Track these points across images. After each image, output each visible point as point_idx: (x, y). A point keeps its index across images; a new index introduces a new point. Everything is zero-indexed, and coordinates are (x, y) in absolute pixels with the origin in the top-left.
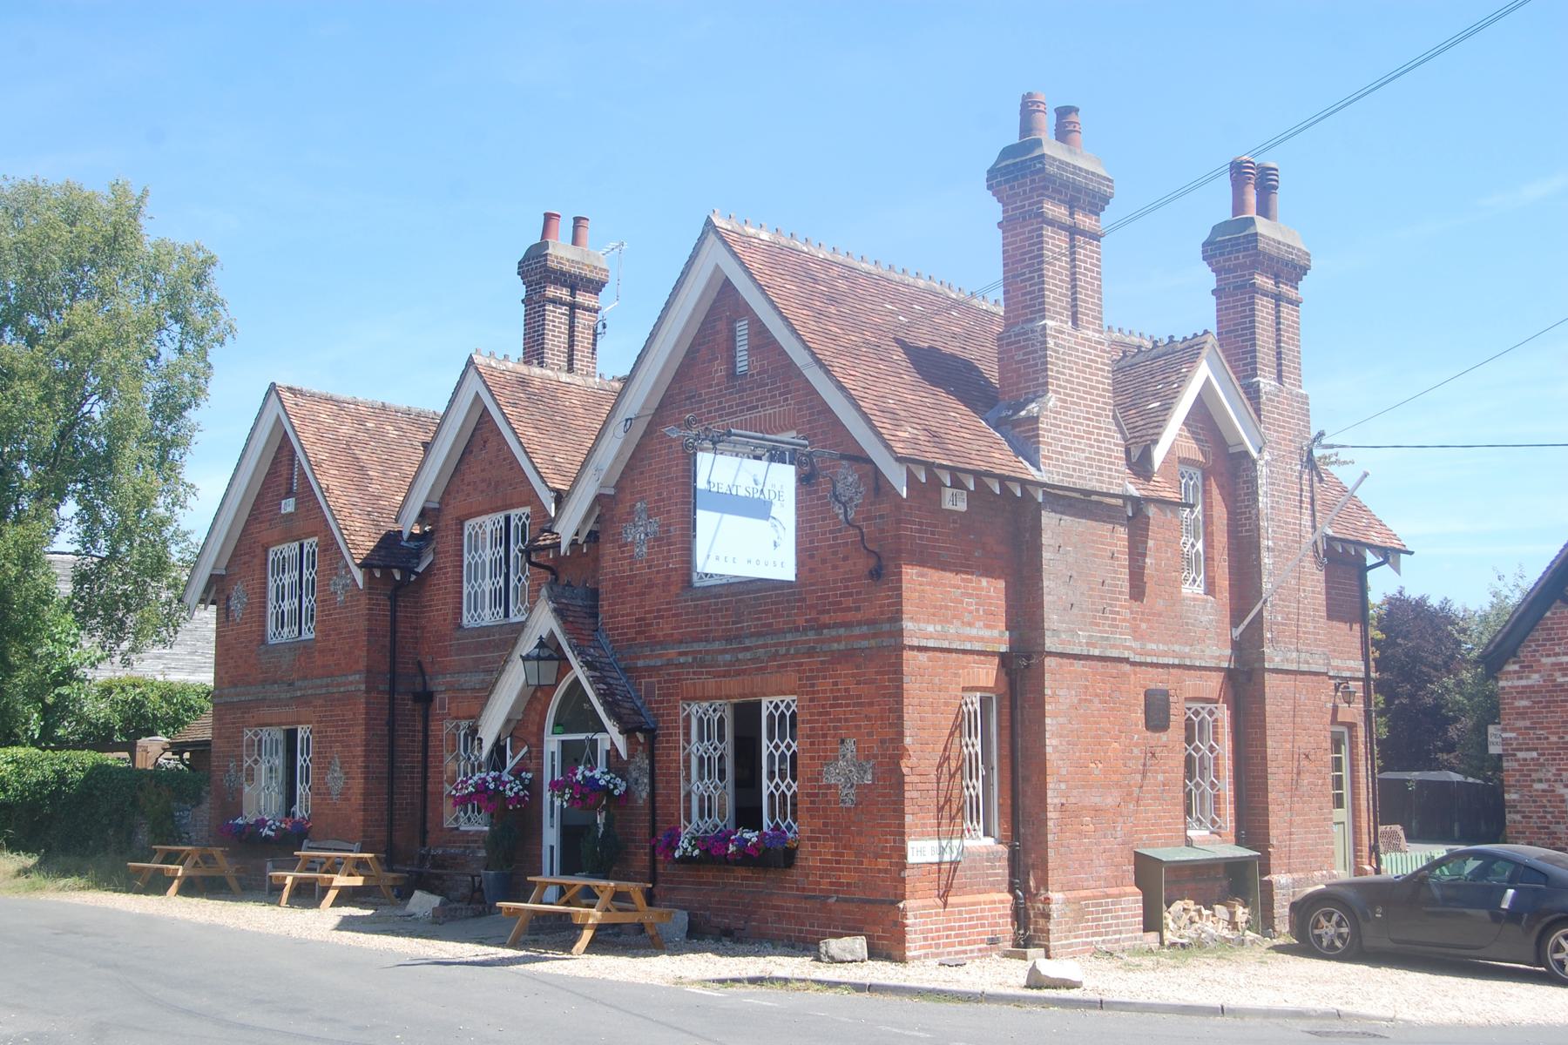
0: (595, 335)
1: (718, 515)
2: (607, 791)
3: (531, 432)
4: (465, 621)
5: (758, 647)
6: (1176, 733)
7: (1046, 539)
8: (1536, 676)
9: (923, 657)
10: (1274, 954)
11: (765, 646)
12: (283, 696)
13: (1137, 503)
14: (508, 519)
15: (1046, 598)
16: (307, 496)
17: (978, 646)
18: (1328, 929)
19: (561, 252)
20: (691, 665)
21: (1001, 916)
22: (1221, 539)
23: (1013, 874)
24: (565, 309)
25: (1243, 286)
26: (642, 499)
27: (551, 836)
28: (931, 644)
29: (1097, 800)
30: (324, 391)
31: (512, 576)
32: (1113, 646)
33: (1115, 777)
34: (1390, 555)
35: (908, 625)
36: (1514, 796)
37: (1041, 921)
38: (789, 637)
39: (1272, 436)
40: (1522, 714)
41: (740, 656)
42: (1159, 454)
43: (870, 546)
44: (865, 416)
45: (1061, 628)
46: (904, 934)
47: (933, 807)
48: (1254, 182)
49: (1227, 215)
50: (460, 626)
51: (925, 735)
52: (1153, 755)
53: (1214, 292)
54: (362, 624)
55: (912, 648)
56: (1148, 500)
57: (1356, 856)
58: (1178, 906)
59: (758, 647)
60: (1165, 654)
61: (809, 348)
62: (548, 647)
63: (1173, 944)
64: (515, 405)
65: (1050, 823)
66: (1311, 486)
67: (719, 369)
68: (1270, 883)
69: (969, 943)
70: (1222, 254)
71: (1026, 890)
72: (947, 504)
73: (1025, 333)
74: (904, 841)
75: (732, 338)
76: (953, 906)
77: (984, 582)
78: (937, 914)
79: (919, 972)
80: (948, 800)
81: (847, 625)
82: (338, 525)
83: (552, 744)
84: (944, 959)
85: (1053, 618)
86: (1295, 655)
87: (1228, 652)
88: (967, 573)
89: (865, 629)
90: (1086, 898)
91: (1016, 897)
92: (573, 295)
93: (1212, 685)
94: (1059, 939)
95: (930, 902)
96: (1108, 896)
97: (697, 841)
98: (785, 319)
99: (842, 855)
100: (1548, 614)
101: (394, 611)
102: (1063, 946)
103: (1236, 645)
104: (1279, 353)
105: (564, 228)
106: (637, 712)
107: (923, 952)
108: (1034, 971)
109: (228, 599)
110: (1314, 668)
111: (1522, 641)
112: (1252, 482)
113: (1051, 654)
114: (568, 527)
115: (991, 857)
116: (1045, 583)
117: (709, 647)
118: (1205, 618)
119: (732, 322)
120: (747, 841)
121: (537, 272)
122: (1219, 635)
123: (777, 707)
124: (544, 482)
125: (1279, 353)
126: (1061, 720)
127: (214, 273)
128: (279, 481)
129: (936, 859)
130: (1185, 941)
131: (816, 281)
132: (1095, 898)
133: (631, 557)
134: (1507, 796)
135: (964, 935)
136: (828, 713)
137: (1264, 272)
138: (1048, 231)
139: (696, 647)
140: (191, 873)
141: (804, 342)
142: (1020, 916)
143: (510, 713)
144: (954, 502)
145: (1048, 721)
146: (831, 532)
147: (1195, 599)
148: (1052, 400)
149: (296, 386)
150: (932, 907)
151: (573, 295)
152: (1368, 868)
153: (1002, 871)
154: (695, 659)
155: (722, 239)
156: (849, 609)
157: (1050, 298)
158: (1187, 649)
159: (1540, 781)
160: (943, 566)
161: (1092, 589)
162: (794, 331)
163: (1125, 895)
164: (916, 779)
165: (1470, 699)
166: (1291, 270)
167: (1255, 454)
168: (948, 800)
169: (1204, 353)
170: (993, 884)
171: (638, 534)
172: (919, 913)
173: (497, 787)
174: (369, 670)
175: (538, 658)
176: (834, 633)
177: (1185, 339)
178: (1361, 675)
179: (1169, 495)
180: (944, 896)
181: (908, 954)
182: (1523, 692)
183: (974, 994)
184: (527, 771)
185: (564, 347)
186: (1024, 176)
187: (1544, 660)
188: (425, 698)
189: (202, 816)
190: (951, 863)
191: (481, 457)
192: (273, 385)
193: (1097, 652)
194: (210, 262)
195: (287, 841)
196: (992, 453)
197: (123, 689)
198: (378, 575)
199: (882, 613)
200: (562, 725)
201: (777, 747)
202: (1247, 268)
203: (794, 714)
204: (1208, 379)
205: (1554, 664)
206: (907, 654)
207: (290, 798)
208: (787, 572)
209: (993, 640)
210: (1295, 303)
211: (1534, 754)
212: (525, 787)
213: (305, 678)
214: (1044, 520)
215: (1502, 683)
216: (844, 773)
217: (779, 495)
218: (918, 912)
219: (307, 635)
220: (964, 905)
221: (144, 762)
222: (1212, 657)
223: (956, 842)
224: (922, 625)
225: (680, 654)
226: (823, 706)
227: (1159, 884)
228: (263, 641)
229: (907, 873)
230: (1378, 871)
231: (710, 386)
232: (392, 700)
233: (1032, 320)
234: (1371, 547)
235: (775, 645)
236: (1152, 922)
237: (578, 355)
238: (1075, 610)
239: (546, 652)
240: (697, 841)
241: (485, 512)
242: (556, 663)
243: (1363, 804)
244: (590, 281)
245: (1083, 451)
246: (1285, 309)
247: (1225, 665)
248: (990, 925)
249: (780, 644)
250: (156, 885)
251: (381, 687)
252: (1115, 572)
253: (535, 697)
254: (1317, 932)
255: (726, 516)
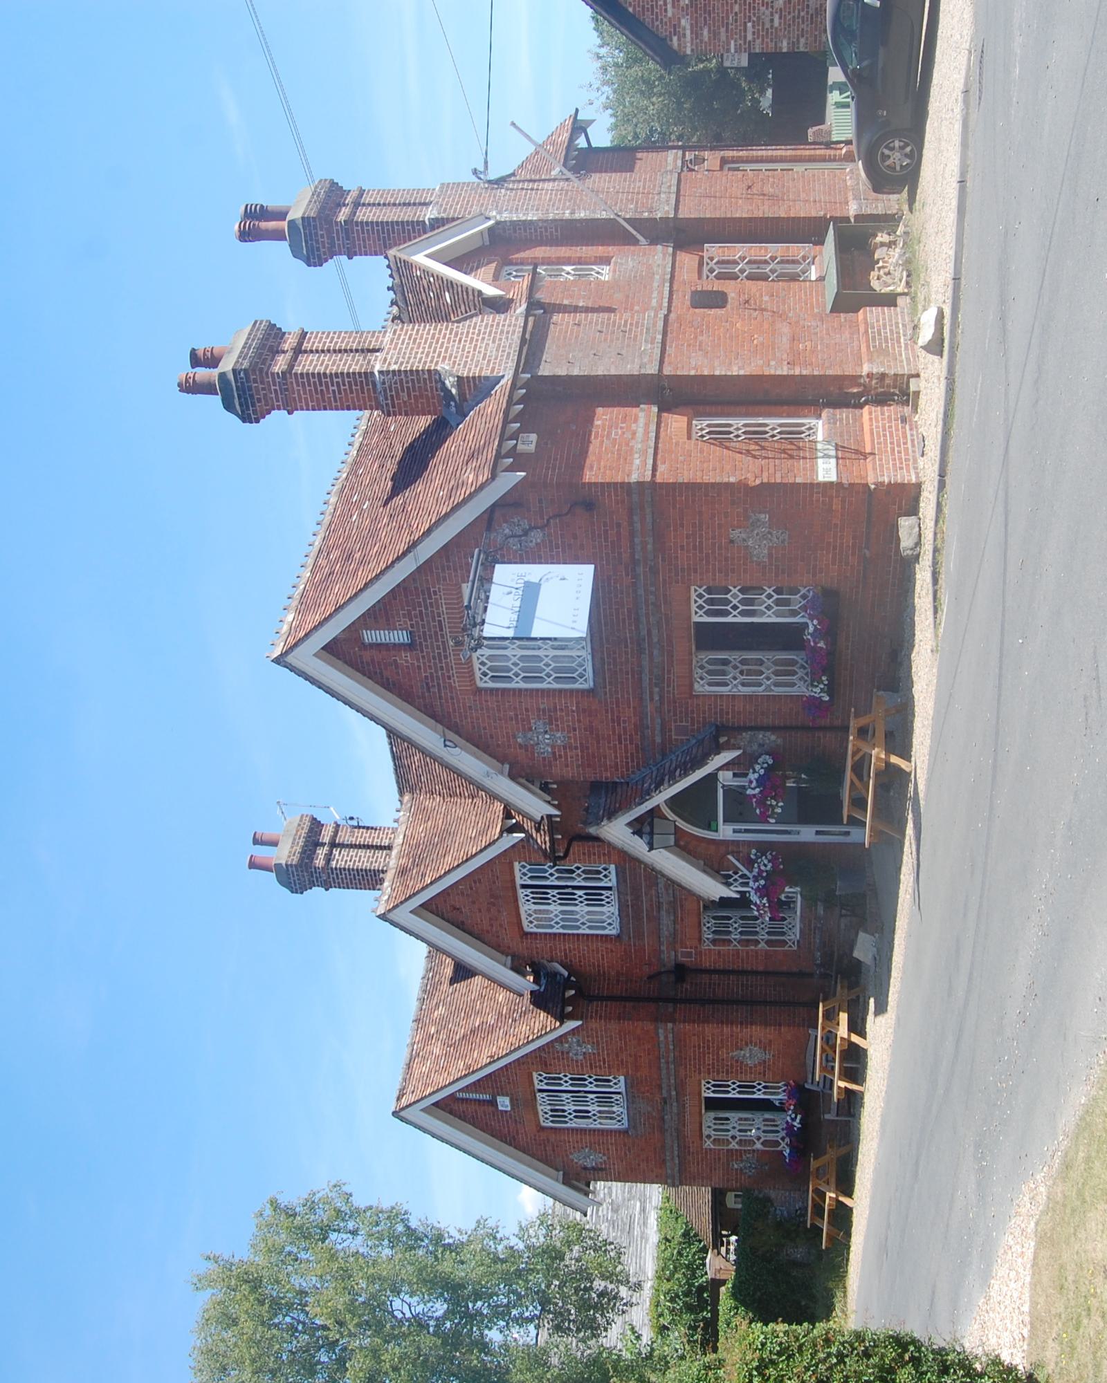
0: (359, 827)
1: (536, 621)
2: (769, 769)
3: (449, 859)
4: (614, 932)
5: (648, 622)
6: (729, 287)
7: (562, 372)
8: (683, 22)
9: (661, 468)
10: (917, 205)
11: (647, 615)
12: (675, 1110)
13: (533, 305)
14: (524, 886)
15: (613, 372)
16: (493, 1082)
17: (653, 427)
18: (896, 158)
19: (285, 854)
20: (662, 689)
21: (883, 414)
22: (564, 251)
23: (847, 406)
24: (336, 852)
25: (347, 231)
26: (514, 737)
27: (807, 834)
28: (650, 462)
29: (784, 339)
30: (401, 1071)
31: (575, 883)
32: (655, 324)
33: (766, 326)
34: (579, 127)
35: (634, 478)
36: (785, 43)
37: (887, 381)
38: (641, 592)
39: (475, 209)
40: (715, 34)
41: (655, 640)
42: (490, 291)
43: (565, 510)
44: (455, 509)
45: (640, 360)
46: (896, 484)
47: (790, 462)
48: (256, 224)
49: (284, 246)
50: (618, 937)
51: (728, 467)
52: (747, 302)
53: (350, 258)
54: (614, 1026)
55: (654, 475)
56: (530, 296)
57: (835, 160)
58: (875, 284)
59: (648, 622)
60: (661, 293)
61: (393, 562)
62: (641, 827)
63: (908, 284)
64: (423, 876)
65: (804, 373)
66: (519, 181)
67: (405, 658)
68: (856, 217)
69: (905, 437)
70: (318, 249)
71: (860, 395)
72: (532, 448)
73: (385, 390)
74: (819, 484)
75: (379, 646)
76: (873, 447)
77: (597, 423)
78: (881, 460)
79: (927, 470)
80: (784, 451)
81: (632, 534)
82: (524, 1045)
83: (726, 832)
84: (918, 455)
85: (630, 368)
86: (663, 196)
87: (659, 247)
88: (590, 435)
89: (636, 518)
90: (868, 347)
91: (866, 403)
92: (323, 845)
93: (687, 261)
94: (902, 367)
95: (870, 466)
96: (866, 332)
97: (814, 680)
98: (366, 585)
99: (829, 543)
100: (631, 10)
101: (601, 998)
102: (908, 364)
103: (654, 241)
104: (404, 204)
105: (263, 852)
106: (700, 742)
107: (912, 472)
108: (928, 348)
109: (585, 1168)
110: (674, 182)
111: (653, 33)
112: (515, 225)
113: (660, 369)
114: (536, 806)
115: (832, 421)
116: (600, 373)
117: (647, 671)
118: (631, 263)
119: (364, 647)
120: (816, 629)
121: (303, 874)
122: (645, 254)
123: (700, 607)
124: (495, 841)
125: (404, 204)
126: (716, 363)
127: (284, 1200)
128: (483, 1111)
129: (833, 461)
130: (905, 274)
131: (331, 573)
132: (868, 341)
133: (565, 748)
134: (785, 50)
135: (898, 441)
136: (707, 555)
137: (336, 214)
138: (298, 369)
139: (646, 678)
140: (833, 1186)
141: (387, 568)
142: (882, 400)
143: (698, 869)
144: (529, 443)
145: (717, 373)
146: (551, 550)
147: (615, 271)
148: (443, 367)
149: (396, 1094)
150: (874, 464)
151: (323, 845)
152: (844, 151)
153: (844, 414)
154: (656, 685)
155: (292, 648)
156: (619, 534)
157: (355, 368)
158: (657, 277)
159: (772, 21)
160: (584, 453)
161: (606, 340)
162: (377, 577)
163: (865, 319)
164: (765, 475)
165: (695, 129)
166: (333, 195)
167: (491, 222)
168: (784, 451)
169: (404, 257)
170: (855, 420)
171: (545, 740)
172: (879, 473)
173: (763, 878)
174: (655, 1019)
175: (651, 834)
176: (638, 548)
177: (391, 276)
178: (680, 153)
179: (526, 283)
180: (865, 456)
181: (914, 481)
182: (696, 34)
183: (948, 385)
184: (749, 854)
185: (369, 853)
186: (250, 388)
187: (670, 14)
188: (681, 971)
189: (780, 1197)
190: (837, 450)
191: (467, 910)
192: (395, 1114)
193: (659, 337)
194: (274, 1204)
195: (808, 1099)
196: (486, 416)
197: (661, 1315)
198: (570, 1009)
199: (623, 502)
200: (710, 824)
201: (735, 608)
202: (327, 231)
203: (709, 591)
204: (427, 256)
205: (673, 6)
206: (659, 479)
207: (765, 1105)
208: (588, 571)
209: (648, 417)
210: (362, 192)
211: (749, 25)
212: (764, 854)
213: (660, 1087)
214: (546, 374)
215: (689, 52)
216: (758, 540)
217: (521, 576)
218: (878, 473)
219: (621, 1087)
220: (873, 441)
221: (729, 1273)
222: (664, 259)
223: (819, 446)
224: (634, 467)
225: (652, 699)
226: (701, 560)
227: (855, 293)
228: (626, 1132)
229: (844, 481)
230: (848, 143)
231: (419, 667)
232: (682, 1001)
233: (374, 384)
234: (572, 139)
235: (647, 606)
236: (890, 300)
237: (377, 842)
238: (623, 352)
239: (647, 829)
240: (814, 680)
241: (517, 908)
242: (656, 820)
243: (789, 153)
244: (311, 830)
245: (487, 344)
246: (366, 199)
247: (670, 250)
248: (890, 421)
249: (646, 601)
250: (843, 1217)
251: (671, 1010)
252: (591, 323)
253: (685, 847)
254: (898, 168)
255: (537, 614)
